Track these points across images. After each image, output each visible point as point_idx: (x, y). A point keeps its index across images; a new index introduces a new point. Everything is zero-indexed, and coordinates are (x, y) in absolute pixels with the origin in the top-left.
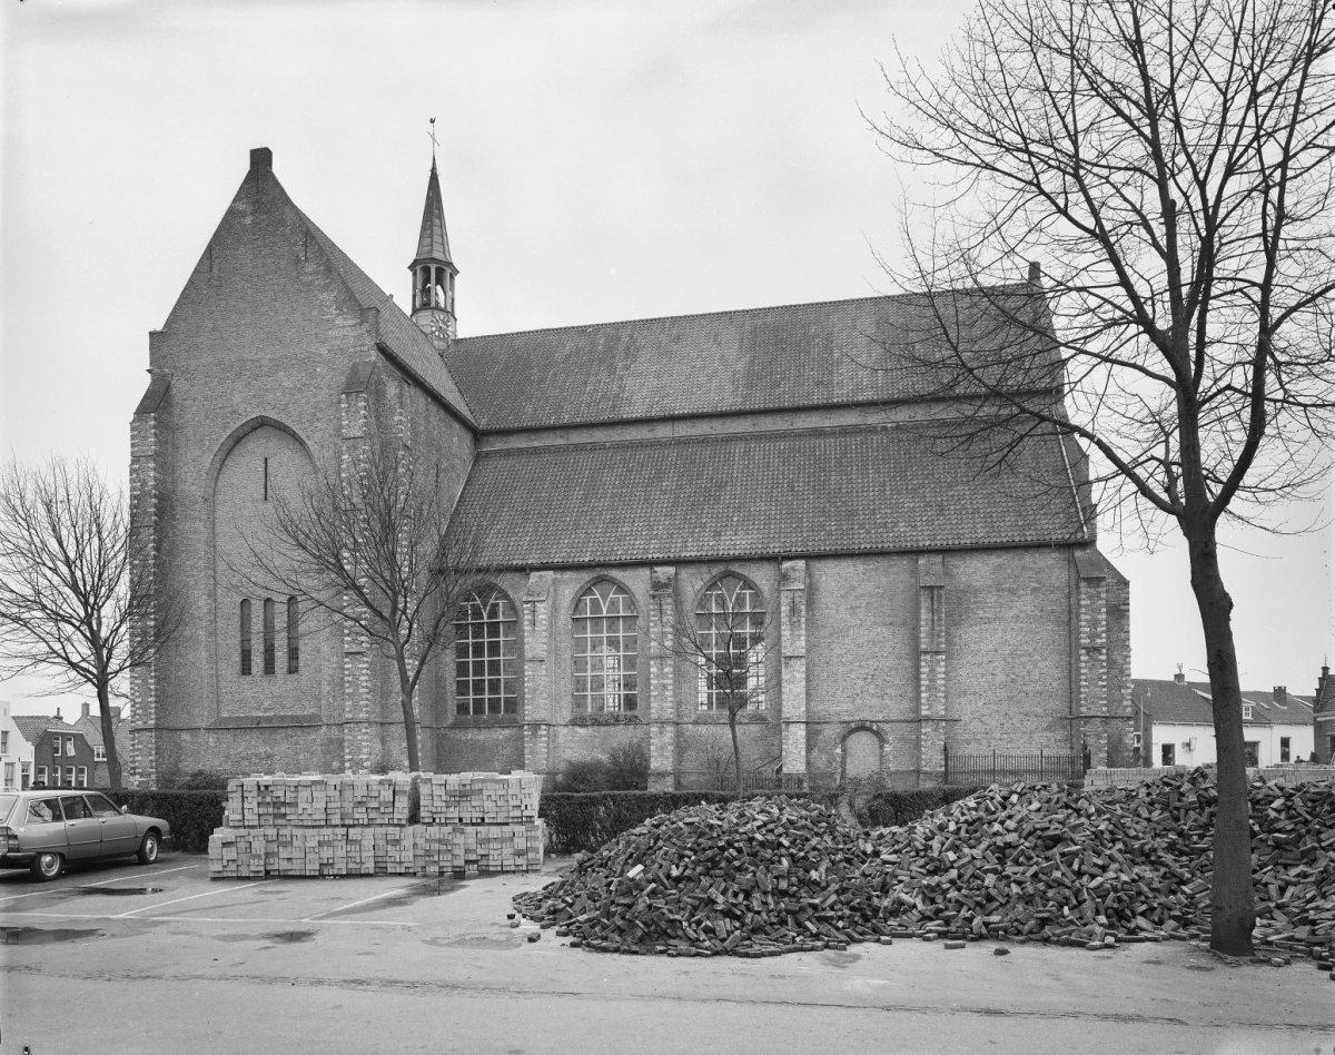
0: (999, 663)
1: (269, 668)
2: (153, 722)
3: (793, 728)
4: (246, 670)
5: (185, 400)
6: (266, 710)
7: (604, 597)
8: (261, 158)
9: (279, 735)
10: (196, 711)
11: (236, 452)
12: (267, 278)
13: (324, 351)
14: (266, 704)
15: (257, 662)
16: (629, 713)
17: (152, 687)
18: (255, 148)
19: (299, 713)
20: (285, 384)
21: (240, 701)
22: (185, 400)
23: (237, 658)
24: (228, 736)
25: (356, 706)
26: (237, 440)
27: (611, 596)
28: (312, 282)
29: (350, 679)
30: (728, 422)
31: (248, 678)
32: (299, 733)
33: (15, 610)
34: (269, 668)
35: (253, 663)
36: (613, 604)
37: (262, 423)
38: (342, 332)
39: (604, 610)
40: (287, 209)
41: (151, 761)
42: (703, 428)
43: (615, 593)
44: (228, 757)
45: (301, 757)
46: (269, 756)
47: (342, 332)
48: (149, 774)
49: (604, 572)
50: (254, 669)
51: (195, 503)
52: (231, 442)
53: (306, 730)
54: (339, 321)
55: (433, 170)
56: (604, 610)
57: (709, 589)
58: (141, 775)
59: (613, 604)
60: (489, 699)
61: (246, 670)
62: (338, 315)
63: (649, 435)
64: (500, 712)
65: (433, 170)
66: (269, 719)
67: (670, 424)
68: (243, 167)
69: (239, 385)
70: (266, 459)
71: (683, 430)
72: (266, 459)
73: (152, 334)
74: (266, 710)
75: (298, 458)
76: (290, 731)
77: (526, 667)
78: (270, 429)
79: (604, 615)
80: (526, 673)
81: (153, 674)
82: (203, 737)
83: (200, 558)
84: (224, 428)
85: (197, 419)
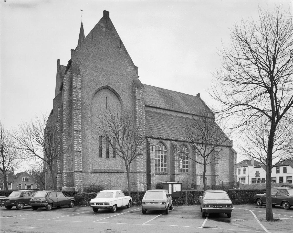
0: (221, 166)
1: (107, 156)
2: (81, 170)
3: (198, 176)
4: (100, 156)
5: (84, 74)
6: (106, 168)
7: (183, 148)
8: (106, 14)
9: (113, 175)
10: (87, 167)
11: (98, 93)
12: (109, 48)
13: (125, 73)
14: (107, 166)
15: (111, 155)
16: (165, 172)
17: (81, 159)
18: (106, 10)
19: (116, 169)
20: (115, 79)
21: (99, 165)
22: (84, 74)
23: (98, 152)
24: (98, 175)
25: (140, 168)
26: (99, 90)
27: (162, 146)
28: (122, 54)
29: (139, 161)
30: (167, 111)
31: (101, 158)
32: (118, 174)
33: (126, 134)
34: (107, 156)
35: (103, 154)
36: (162, 148)
37: (107, 88)
38: (130, 70)
39: (160, 149)
40: (115, 31)
41: (81, 182)
42: (162, 111)
43: (185, 148)
44: (97, 181)
45: (119, 181)
46: (110, 181)
47: (130, 70)
48: (80, 186)
49: (162, 140)
50: (103, 156)
51: (87, 105)
52: (98, 90)
53: (120, 174)
54: (129, 67)
55: (82, 24)
56: (160, 149)
57: (157, 145)
58: (78, 186)
59: (162, 148)
60: (164, 168)
61: (100, 156)
62: (129, 66)
63: (152, 110)
64: (163, 171)
65: (82, 24)
66: (109, 170)
67: (156, 109)
68: (102, 15)
69: (101, 75)
70: (107, 98)
71: (159, 111)
72: (107, 98)
73: (72, 50)
74: (106, 168)
75: (117, 101)
76: (116, 174)
77: (151, 161)
78: (108, 90)
79: (160, 150)
80: (151, 162)
81: (81, 155)
82: (89, 174)
83: (89, 122)
84: (97, 85)
85: (88, 81)
